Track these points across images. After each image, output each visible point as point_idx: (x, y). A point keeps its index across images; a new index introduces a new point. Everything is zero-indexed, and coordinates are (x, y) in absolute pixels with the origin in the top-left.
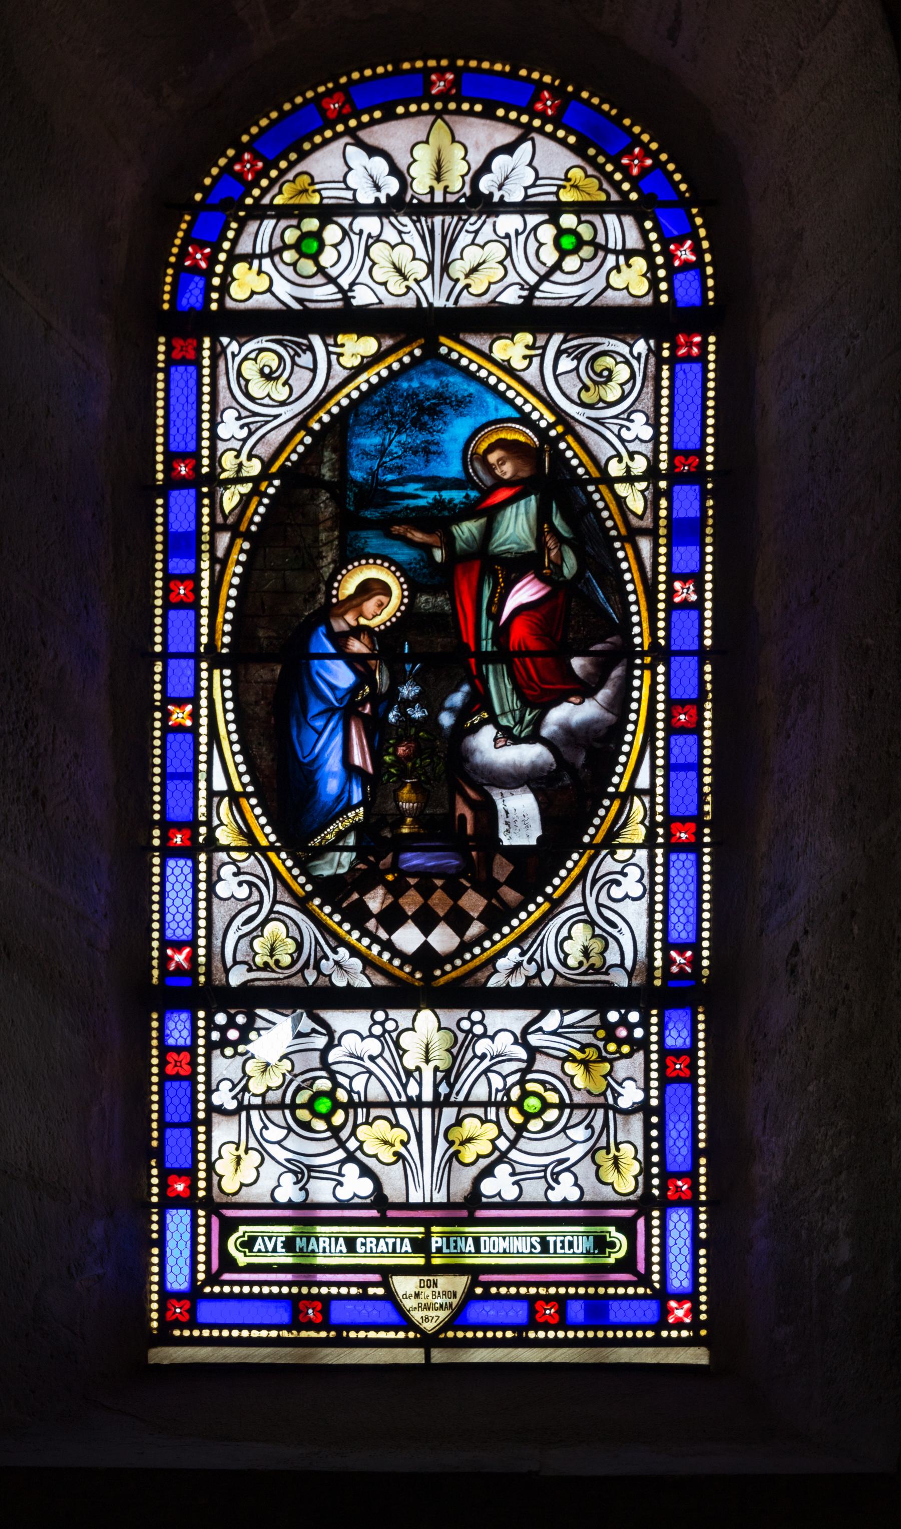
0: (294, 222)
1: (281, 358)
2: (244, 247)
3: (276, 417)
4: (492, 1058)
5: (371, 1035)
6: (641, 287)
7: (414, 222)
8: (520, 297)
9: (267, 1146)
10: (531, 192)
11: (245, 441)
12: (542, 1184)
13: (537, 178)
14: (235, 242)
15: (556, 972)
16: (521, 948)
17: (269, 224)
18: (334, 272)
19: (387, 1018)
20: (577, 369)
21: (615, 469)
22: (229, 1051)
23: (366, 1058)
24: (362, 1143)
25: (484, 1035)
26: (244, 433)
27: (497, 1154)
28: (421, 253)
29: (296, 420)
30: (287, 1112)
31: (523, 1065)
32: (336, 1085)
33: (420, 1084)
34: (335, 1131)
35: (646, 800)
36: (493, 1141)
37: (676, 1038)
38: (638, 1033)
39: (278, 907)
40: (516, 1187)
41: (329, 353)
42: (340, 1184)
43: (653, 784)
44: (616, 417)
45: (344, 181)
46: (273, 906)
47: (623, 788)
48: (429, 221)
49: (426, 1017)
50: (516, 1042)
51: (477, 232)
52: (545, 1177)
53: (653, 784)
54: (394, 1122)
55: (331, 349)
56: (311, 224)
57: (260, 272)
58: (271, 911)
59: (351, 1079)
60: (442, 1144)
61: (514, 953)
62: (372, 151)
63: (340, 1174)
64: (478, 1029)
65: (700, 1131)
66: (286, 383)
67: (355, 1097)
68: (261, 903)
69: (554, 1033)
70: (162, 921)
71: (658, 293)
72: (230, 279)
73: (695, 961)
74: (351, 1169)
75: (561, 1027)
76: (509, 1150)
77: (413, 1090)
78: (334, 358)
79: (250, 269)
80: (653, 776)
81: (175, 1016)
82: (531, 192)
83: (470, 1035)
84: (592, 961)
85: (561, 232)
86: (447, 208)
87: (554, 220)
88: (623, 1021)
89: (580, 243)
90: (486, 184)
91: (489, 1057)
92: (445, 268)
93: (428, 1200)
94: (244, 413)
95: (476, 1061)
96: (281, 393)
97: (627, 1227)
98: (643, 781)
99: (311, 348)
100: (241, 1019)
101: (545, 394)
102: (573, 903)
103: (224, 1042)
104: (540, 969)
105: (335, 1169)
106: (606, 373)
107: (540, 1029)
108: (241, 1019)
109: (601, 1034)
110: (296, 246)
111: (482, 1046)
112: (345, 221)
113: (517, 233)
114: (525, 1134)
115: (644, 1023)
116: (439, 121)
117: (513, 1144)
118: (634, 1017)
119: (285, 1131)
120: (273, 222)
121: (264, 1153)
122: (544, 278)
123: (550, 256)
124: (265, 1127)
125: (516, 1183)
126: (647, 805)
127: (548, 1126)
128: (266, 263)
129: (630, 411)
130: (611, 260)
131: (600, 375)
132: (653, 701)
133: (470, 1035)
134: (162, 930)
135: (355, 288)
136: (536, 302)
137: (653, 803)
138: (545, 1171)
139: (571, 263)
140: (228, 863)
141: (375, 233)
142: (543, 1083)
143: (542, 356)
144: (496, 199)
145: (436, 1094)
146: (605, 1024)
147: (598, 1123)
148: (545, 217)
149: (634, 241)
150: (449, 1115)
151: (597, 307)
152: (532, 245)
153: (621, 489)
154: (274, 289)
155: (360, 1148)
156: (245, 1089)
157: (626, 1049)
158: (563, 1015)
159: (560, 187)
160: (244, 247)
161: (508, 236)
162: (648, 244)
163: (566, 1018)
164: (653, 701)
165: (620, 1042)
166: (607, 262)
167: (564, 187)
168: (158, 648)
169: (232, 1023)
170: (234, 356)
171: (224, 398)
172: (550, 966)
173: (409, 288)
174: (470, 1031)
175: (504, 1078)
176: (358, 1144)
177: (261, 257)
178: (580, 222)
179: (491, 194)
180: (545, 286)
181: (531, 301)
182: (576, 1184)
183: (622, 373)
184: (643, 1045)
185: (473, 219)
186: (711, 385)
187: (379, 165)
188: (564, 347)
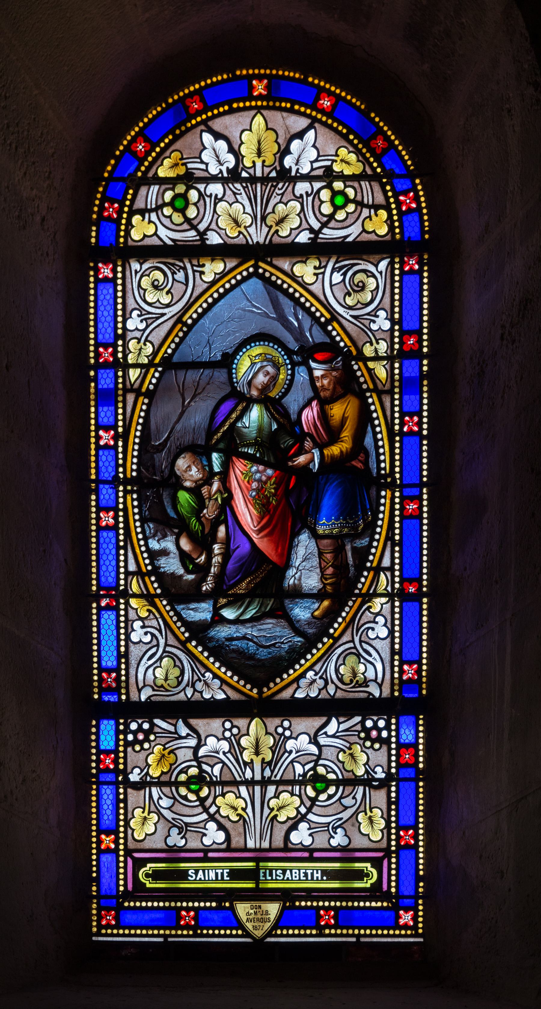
0: (171, 186)
1: (165, 275)
2: (140, 204)
3: (163, 315)
4: (297, 752)
5: (225, 739)
6: (383, 230)
7: (244, 188)
8: (309, 239)
9: (162, 811)
10: (316, 165)
11: (144, 330)
12: (327, 836)
13: (319, 155)
14: (133, 201)
15: (337, 687)
16: (314, 671)
17: (155, 189)
18: (195, 222)
19: (233, 726)
20: (344, 280)
21: (368, 351)
22: (137, 748)
23: (221, 753)
24: (219, 808)
25: (290, 737)
26: (143, 325)
27: (299, 816)
28: (249, 209)
29: (176, 317)
30: (173, 789)
31: (315, 758)
32: (201, 771)
33: (253, 771)
34: (202, 801)
35: (389, 574)
36: (297, 809)
37: (407, 736)
38: (384, 734)
39: (168, 649)
40: (311, 838)
41: (194, 271)
42: (205, 835)
43: (393, 563)
44: (368, 314)
45: (200, 157)
46: (165, 648)
47: (375, 564)
48: (254, 186)
49: (255, 725)
50: (310, 742)
51: (282, 194)
52: (328, 830)
53: (393, 563)
54: (238, 795)
55: (195, 268)
56: (181, 188)
57: (150, 222)
58: (164, 651)
59: (212, 767)
60: (266, 811)
61: (310, 674)
62: (217, 136)
63: (205, 828)
64: (288, 733)
65: (398, 570)
66: (168, 292)
67: (214, 779)
68: (158, 645)
69: (333, 736)
70: (99, 656)
71: (394, 234)
72: (130, 227)
73: (419, 671)
74: (212, 826)
75: (337, 732)
76: (307, 814)
77: (248, 774)
78: (197, 274)
79: (143, 220)
80: (393, 558)
81: (105, 722)
82: (316, 165)
83: (283, 737)
84: (357, 678)
85: (335, 194)
86: (264, 180)
87: (329, 186)
88: (375, 727)
89: (348, 201)
90: (288, 161)
91: (294, 752)
92: (264, 218)
93: (258, 846)
94: (144, 312)
95: (287, 754)
96: (166, 300)
97: (377, 863)
98: (386, 562)
99: (185, 269)
100: (146, 726)
101: (325, 302)
102: (344, 641)
103: (136, 741)
104: (326, 683)
105: (202, 825)
106: (361, 284)
107: (325, 733)
108: (146, 726)
109: (363, 735)
110: (171, 204)
111: (290, 745)
112: (201, 187)
113: (308, 195)
114: (317, 803)
115: (388, 727)
116: (259, 115)
117: (309, 810)
118: (381, 724)
119: (173, 800)
120: (157, 187)
121: (160, 814)
122: (324, 225)
123: (327, 209)
124: (160, 798)
125: (310, 835)
126: (389, 578)
127: (330, 797)
128: (154, 217)
129: (377, 309)
130: (365, 212)
131: (357, 286)
132: (392, 516)
133: (283, 737)
134: (99, 662)
135: (208, 233)
136: (319, 241)
137: (393, 576)
138: (328, 827)
139: (340, 215)
140: (137, 620)
141: (220, 196)
142: (324, 766)
143: (323, 273)
144: (293, 173)
145: (263, 777)
146: (365, 729)
147: (359, 796)
148: (324, 184)
149: (380, 199)
150: (271, 790)
151: (359, 242)
152: (317, 202)
153: (371, 364)
154: (158, 233)
155: (218, 811)
156: (147, 774)
157: (377, 746)
158: (339, 723)
159: (334, 161)
160: (140, 204)
161: (301, 196)
162: (389, 204)
163: (341, 726)
164: (392, 516)
165: (373, 741)
166: (362, 214)
167: (336, 161)
168: (93, 477)
169: (140, 729)
170: (136, 272)
171: (131, 304)
172: (333, 682)
173: (240, 233)
174: (283, 734)
175: (303, 766)
176: (217, 808)
177: (150, 211)
178: (346, 187)
179: (290, 167)
180: (325, 231)
181: (317, 240)
182: (346, 835)
183: (371, 283)
184: (387, 742)
185: (280, 185)
186: (425, 287)
187: (222, 145)
188: (337, 266)
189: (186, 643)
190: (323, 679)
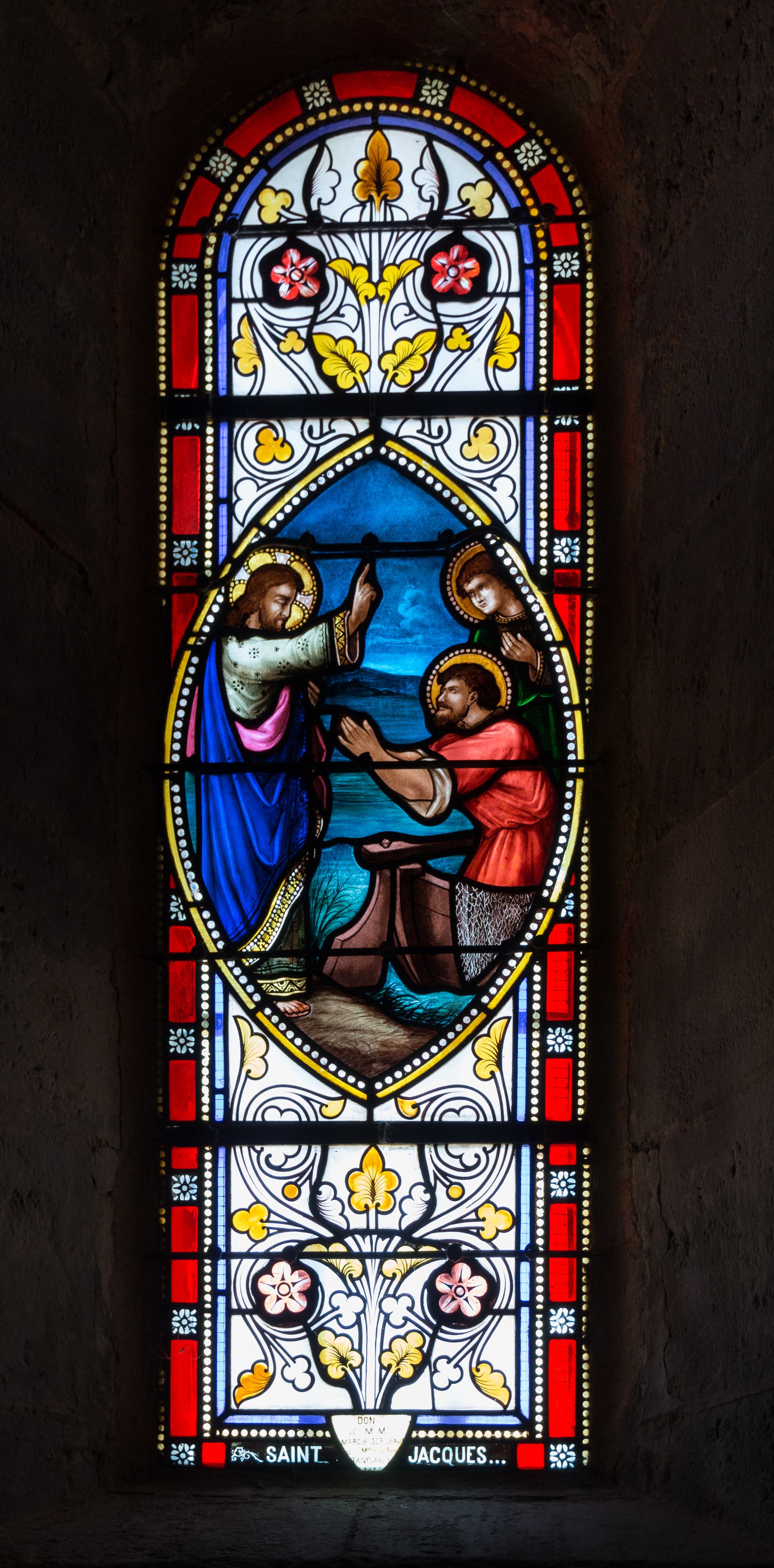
105: (423, 1107)
189: (489, 1009)
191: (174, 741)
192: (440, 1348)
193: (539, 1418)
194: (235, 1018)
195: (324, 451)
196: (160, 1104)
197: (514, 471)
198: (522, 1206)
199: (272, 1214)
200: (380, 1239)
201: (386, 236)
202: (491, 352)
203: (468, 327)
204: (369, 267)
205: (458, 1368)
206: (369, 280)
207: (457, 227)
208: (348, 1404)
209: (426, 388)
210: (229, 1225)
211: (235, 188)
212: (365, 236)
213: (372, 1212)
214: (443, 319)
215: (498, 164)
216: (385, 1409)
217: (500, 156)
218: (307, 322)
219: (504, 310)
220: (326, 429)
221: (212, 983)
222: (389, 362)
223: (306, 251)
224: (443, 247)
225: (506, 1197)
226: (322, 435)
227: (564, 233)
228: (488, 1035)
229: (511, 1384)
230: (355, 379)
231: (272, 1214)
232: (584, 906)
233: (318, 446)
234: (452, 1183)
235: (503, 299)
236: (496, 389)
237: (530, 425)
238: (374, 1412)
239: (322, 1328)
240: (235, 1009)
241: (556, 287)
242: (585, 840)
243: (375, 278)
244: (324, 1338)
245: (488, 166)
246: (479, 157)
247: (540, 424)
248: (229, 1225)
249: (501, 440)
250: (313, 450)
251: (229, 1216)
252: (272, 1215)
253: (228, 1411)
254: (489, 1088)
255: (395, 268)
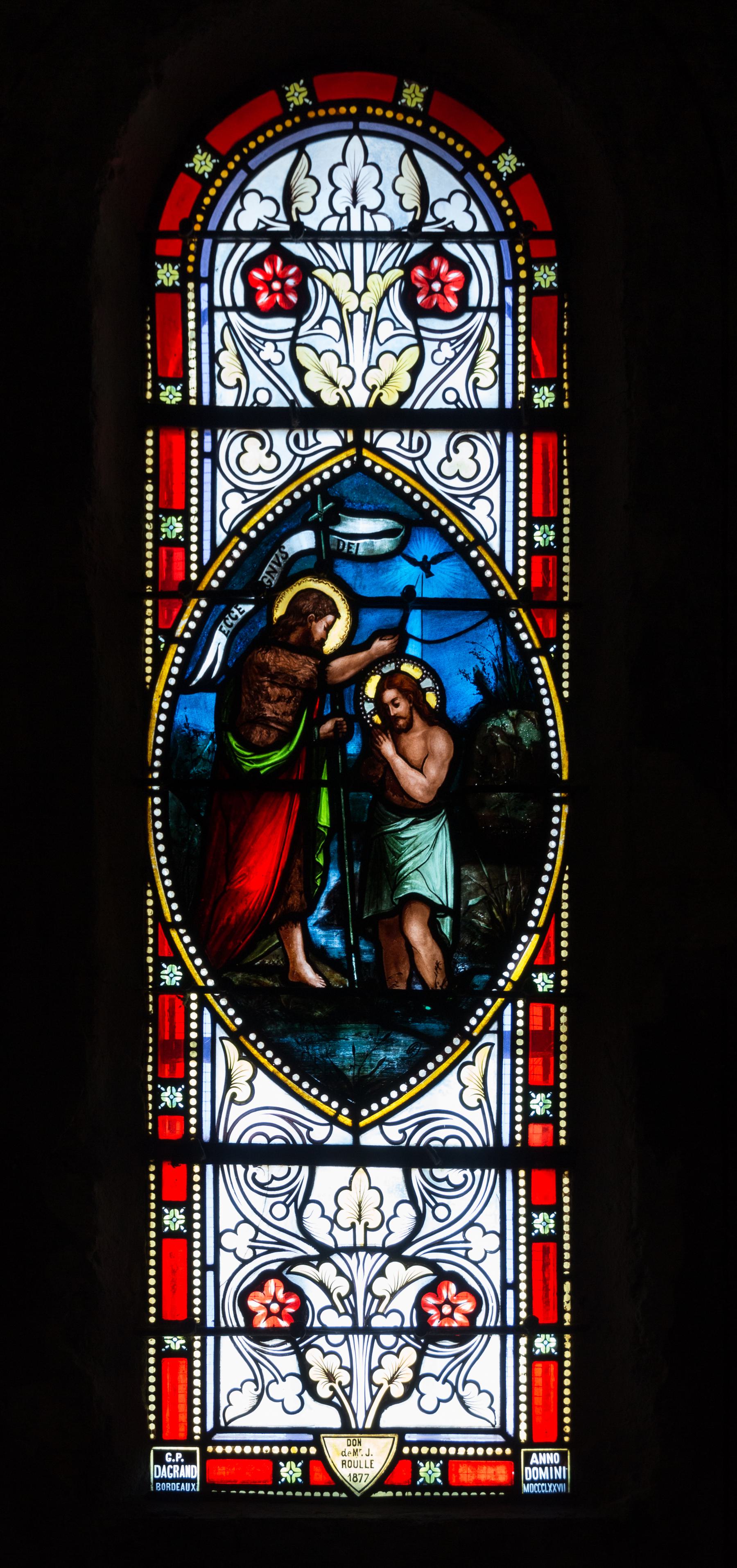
152: (275, 1184)
190: (376, 1385)
191: (157, 733)
192: (430, 1365)
193: (522, 572)
194: (221, 1039)
195: (308, 461)
196: (153, 1220)
197: (494, 493)
198: (507, 513)
199: (260, 1233)
200: (369, 1255)
201: (371, 247)
202: (471, 370)
203: (463, 1252)
204: (350, 273)
205: (447, 1384)
206: (352, 289)
207: (437, 239)
208: (337, 1423)
209: (407, 405)
210: (218, 1245)
211: (218, 183)
212: (346, 247)
213: (360, 1228)
214: (424, 334)
215: (479, 176)
216: (376, 1430)
217: (481, 167)
218: (289, 334)
219: (486, 324)
220: (311, 441)
221: (200, 1012)
222: (372, 377)
223: (290, 259)
224: (423, 260)
225: (491, 1219)
226: (307, 447)
227: (541, 248)
228: (473, 1063)
229: (497, 1405)
230: (338, 394)
231: (260, 1233)
232: (563, 1105)
233: (304, 457)
234: (437, 1205)
235: (484, 314)
236: (476, 406)
237: (510, 440)
238: (364, 1431)
239: (309, 1346)
240: (220, 1032)
241: (535, 299)
242: (565, 887)
243: (359, 288)
244: (312, 1356)
245: (469, 178)
246: (459, 167)
247: (520, 441)
248: (218, 1245)
249: (483, 456)
250: (299, 460)
251: (218, 1236)
252: (260, 1234)
253: (217, 1429)
254: (476, 1117)
255: (379, 276)
